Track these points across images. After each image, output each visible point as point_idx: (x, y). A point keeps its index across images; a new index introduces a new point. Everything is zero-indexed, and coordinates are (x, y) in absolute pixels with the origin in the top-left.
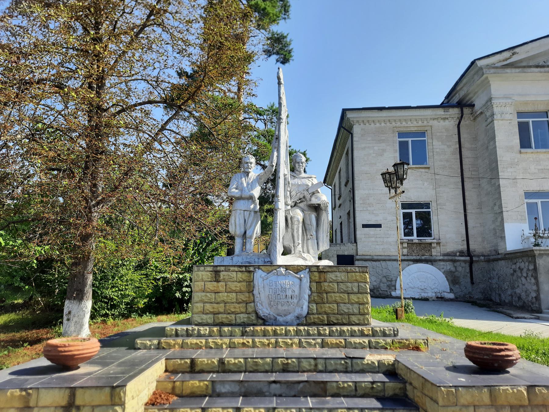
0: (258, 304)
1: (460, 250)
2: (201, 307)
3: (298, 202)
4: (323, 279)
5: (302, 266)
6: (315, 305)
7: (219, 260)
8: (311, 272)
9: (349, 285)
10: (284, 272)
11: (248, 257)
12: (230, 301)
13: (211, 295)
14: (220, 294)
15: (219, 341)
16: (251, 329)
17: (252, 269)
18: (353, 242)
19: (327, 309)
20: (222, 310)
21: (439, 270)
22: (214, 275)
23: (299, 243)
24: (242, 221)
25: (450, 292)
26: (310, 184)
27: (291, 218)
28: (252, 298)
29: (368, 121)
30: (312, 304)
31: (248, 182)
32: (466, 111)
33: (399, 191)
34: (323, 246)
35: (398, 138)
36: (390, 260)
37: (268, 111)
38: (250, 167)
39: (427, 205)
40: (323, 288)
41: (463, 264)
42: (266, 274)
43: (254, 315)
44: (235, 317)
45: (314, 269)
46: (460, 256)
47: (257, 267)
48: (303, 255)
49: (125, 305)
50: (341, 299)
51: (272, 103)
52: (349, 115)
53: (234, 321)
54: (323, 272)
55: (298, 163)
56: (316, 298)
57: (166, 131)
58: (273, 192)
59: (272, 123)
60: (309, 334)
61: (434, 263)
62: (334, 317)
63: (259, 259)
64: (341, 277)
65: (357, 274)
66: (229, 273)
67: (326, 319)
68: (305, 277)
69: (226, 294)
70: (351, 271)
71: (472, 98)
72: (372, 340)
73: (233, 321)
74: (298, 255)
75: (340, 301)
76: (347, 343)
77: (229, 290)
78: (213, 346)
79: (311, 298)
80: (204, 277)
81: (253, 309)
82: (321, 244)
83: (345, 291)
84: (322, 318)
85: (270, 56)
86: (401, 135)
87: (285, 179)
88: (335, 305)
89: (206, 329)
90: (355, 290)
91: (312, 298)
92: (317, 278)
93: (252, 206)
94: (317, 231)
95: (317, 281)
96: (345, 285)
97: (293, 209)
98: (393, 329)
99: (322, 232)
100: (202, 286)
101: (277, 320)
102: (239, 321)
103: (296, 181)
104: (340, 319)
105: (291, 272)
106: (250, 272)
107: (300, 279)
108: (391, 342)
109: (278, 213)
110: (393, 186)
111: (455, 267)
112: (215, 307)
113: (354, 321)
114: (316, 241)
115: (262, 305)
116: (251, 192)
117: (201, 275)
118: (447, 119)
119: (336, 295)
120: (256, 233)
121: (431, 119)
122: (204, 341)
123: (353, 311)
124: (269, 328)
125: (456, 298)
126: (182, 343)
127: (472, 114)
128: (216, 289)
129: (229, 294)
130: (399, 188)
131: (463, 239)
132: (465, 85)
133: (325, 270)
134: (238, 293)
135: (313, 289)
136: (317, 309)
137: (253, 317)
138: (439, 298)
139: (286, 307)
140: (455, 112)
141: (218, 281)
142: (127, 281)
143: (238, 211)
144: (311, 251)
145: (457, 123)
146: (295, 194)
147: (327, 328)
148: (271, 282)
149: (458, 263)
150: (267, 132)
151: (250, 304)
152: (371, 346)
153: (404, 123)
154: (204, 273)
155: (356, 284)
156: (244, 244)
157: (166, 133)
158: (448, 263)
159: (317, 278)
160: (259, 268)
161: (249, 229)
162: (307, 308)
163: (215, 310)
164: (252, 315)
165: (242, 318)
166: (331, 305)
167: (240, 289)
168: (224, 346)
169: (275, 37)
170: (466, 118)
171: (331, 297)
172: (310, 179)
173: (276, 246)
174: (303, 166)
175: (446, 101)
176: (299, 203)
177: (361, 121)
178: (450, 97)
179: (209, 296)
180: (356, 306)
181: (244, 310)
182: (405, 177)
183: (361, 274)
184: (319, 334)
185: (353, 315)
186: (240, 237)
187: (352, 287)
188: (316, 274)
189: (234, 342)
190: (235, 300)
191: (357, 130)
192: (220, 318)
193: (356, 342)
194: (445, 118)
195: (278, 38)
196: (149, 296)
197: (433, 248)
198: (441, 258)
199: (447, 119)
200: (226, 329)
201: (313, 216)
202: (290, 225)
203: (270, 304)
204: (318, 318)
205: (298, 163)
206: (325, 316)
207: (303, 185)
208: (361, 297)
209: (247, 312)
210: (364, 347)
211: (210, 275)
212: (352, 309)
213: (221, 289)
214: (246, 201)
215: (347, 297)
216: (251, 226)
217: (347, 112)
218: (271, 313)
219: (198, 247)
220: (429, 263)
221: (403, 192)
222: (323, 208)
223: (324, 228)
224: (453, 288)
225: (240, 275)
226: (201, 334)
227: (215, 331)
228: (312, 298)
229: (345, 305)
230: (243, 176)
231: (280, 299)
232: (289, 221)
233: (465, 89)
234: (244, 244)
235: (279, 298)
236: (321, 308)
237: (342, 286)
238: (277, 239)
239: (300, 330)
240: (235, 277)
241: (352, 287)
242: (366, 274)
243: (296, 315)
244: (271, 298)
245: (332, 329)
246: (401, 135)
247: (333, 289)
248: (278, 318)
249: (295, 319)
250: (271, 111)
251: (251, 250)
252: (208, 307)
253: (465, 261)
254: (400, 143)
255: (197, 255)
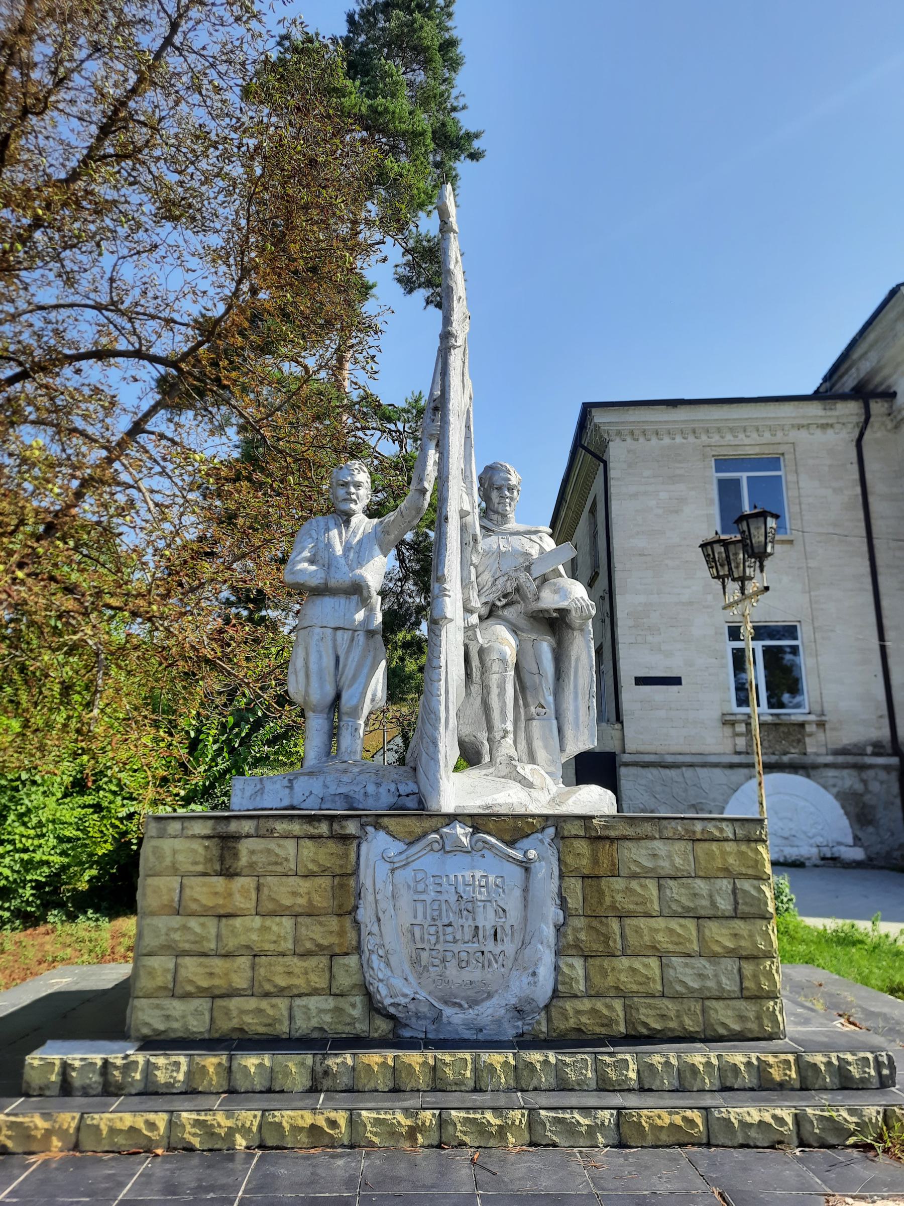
0: (374, 957)
1: (875, 739)
2: (168, 970)
3: (499, 604)
4: (605, 864)
5: (533, 816)
6: (578, 963)
7: (249, 790)
8: (563, 838)
9: (701, 885)
10: (465, 841)
11: (345, 778)
12: (272, 947)
13: (203, 925)
14: (238, 922)
15: (220, 1118)
16: (344, 1063)
17: (351, 828)
18: (613, 718)
19: (623, 978)
20: (240, 982)
21: (825, 787)
22: (216, 852)
23: (506, 732)
24: (329, 662)
25: (855, 845)
26: (535, 551)
27: (482, 652)
28: (351, 935)
29: (644, 433)
30: (570, 960)
31: (346, 543)
32: (877, 407)
33: (751, 587)
34: (576, 738)
35: (717, 471)
36: (704, 765)
37: (408, 411)
38: (354, 497)
39: (790, 631)
40: (608, 900)
41: (883, 775)
42: (402, 846)
43: (358, 1000)
44: (291, 1008)
45: (574, 829)
46: (875, 754)
47: (369, 819)
48: (519, 769)
49: (32, 888)
50: (675, 939)
51: (417, 393)
52: (599, 417)
53: (286, 1023)
54: (608, 838)
55: (499, 489)
56: (583, 936)
57: (145, 435)
58: (418, 600)
59: (415, 440)
60: (563, 1086)
61: (812, 773)
62: (649, 1006)
63: (378, 785)
64: (670, 857)
65: (730, 847)
66: (272, 845)
67: (621, 1014)
68: (541, 858)
69: (257, 921)
70: (706, 836)
71: (890, 376)
72: (809, 1111)
73: (280, 1022)
74: (504, 770)
75: (671, 947)
76: (715, 1127)
77: (270, 906)
78: (196, 1142)
79: (565, 935)
80: (180, 858)
81: (356, 979)
82: (569, 733)
83: (688, 909)
84: (605, 1011)
85: (410, 291)
86: (722, 464)
87: (463, 528)
88: (654, 963)
89: (177, 1064)
90: (725, 905)
91: (570, 938)
92: (585, 863)
93: (360, 616)
94: (558, 692)
95: (586, 872)
96: (687, 887)
97: (485, 624)
98: (876, 1059)
99: (572, 696)
100: (171, 890)
101: (445, 1020)
102: (302, 1026)
103: (492, 542)
104: (672, 1014)
105: (493, 840)
106: (345, 839)
107: (526, 866)
108: (880, 1118)
109: (443, 633)
110: (736, 576)
111: (865, 782)
112: (217, 971)
113: (723, 1024)
114: (555, 722)
115: (388, 964)
116: (358, 571)
117: (168, 852)
118: (832, 426)
119: (652, 922)
120: (373, 700)
121: (793, 426)
122: (161, 1120)
123: (719, 983)
124: (414, 1058)
125: (870, 859)
126: (78, 1129)
127: (889, 415)
128: (221, 902)
129: (268, 922)
130: (750, 578)
131: (880, 713)
132: (871, 346)
133: (612, 834)
134: (300, 919)
135: (571, 903)
136: (587, 978)
137: (355, 1008)
138: (828, 859)
139: (473, 974)
140: (850, 410)
141: (228, 873)
142: (40, 824)
143: (317, 630)
144: (541, 754)
145: (856, 434)
146: (491, 579)
147: (628, 1057)
148: (420, 876)
149: (870, 773)
150: (406, 461)
151: (346, 960)
152: (806, 1136)
153: (729, 437)
154: (179, 844)
155: (725, 885)
156: (334, 733)
157: (142, 438)
158: (845, 772)
159: (585, 863)
160: (377, 826)
161: (350, 686)
162: (553, 975)
163: (217, 982)
164: (352, 999)
165: (314, 1012)
166: (637, 964)
167: (310, 901)
168: (241, 1142)
169: (424, 247)
170: (877, 425)
171: (637, 931)
172: (533, 537)
173: (435, 744)
174: (512, 499)
175: (828, 384)
176: (504, 607)
177: (626, 432)
178: (835, 378)
179: (198, 930)
180: (730, 964)
181: (320, 982)
182: (769, 550)
183: (744, 847)
184: (604, 1086)
185: (718, 998)
186: (321, 712)
187: (711, 896)
188: (582, 847)
189: (279, 1125)
190: (290, 945)
191: (617, 452)
192: (235, 1013)
193: (749, 1119)
194: (827, 424)
195: (431, 249)
196: (103, 862)
197: (810, 735)
198: (829, 759)
199: (832, 426)
200: (251, 1062)
201: (545, 648)
202: (476, 674)
203: (416, 961)
204: (594, 1011)
205: (499, 489)
206: (618, 1005)
207: (515, 553)
208: (745, 933)
209: (334, 990)
210: (780, 1142)
211: (201, 850)
212: (716, 976)
213: (241, 902)
214: (342, 600)
215: (694, 933)
216: (354, 678)
217: (593, 410)
218: (422, 995)
219: (230, 733)
220: (801, 772)
221: (767, 589)
222: (577, 622)
223: (581, 681)
224: (860, 834)
225: (309, 849)
226: (155, 1083)
227: (211, 1070)
228: (570, 938)
229: (688, 960)
230: (331, 523)
231: (455, 941)
232: (475, 662)
233: (873, 357)
234: (334, 733)
235: (450, 938)
236: (604, 973)
237: (674, 889)
238: (438, 719)
239: (530, 1066)
240: (292, 859)
241: (711, 896)
242: (761, 848)
243: (513, 1001)
244: (422, 939)
245: (647, 1060)
246: (722, 464)
247: (642, 903)
248: (448, 1011)
249: (509, 1015)
250: (414, 411)
251: (355, 752)
252: (192, 969)
253: (887, 768)
254: (722, 483)
255: (225, 754)
